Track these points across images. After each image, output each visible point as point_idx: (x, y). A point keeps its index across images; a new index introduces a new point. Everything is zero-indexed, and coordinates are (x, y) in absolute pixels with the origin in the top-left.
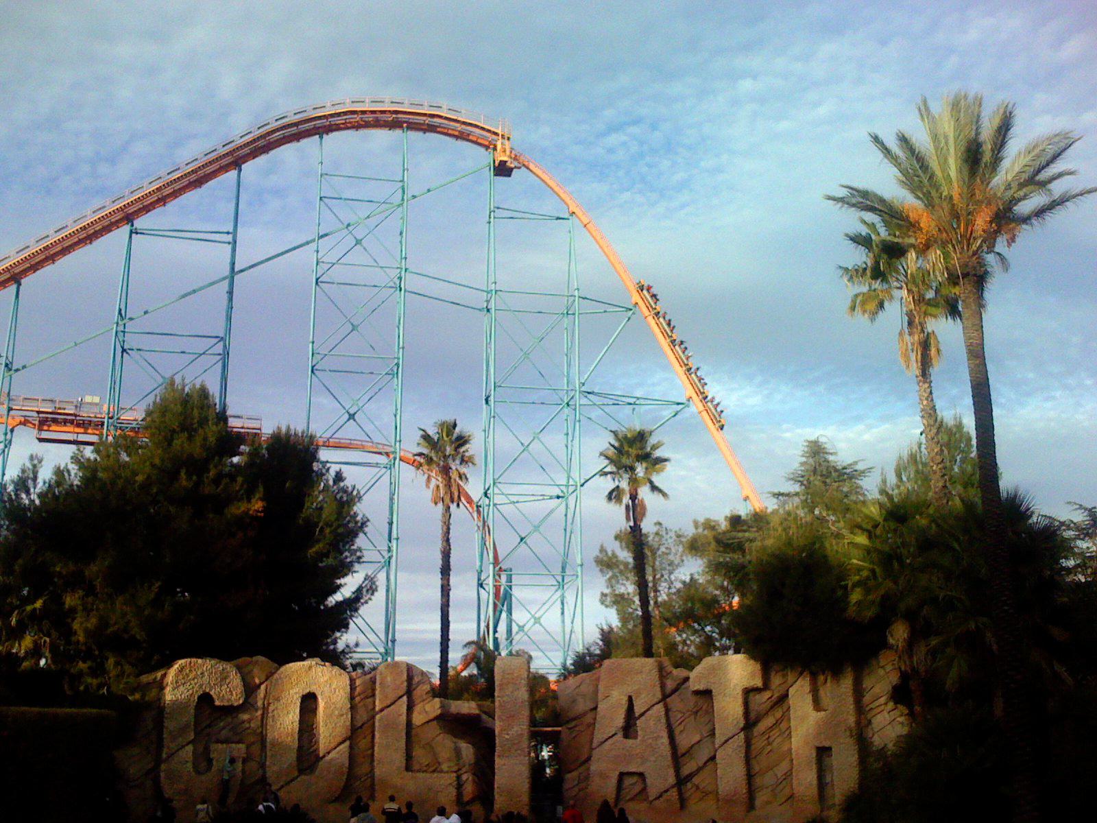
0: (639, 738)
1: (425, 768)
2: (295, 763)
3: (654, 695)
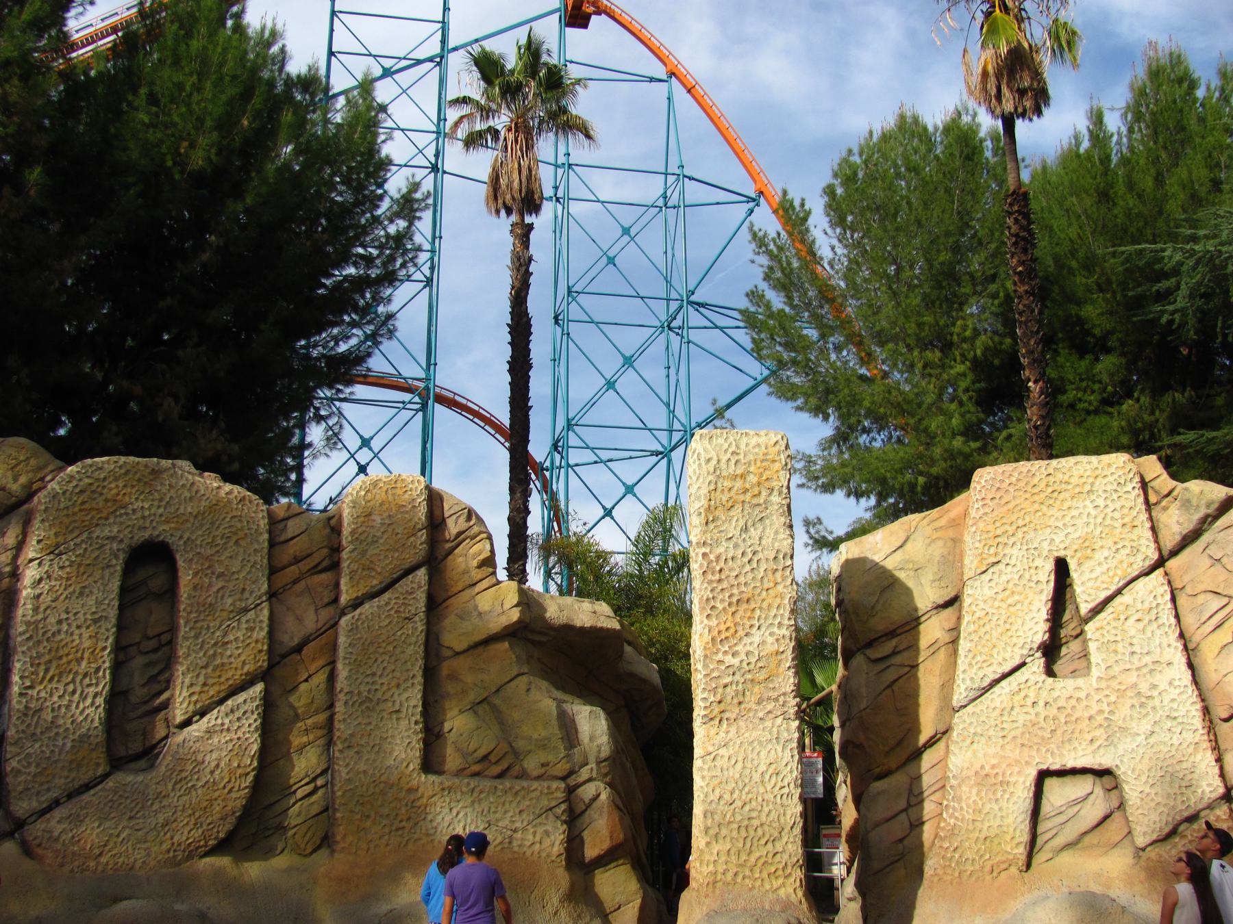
0: (1095, 672)
1: (476, 768)
2: (99, 735)
3: (1135, 550)
